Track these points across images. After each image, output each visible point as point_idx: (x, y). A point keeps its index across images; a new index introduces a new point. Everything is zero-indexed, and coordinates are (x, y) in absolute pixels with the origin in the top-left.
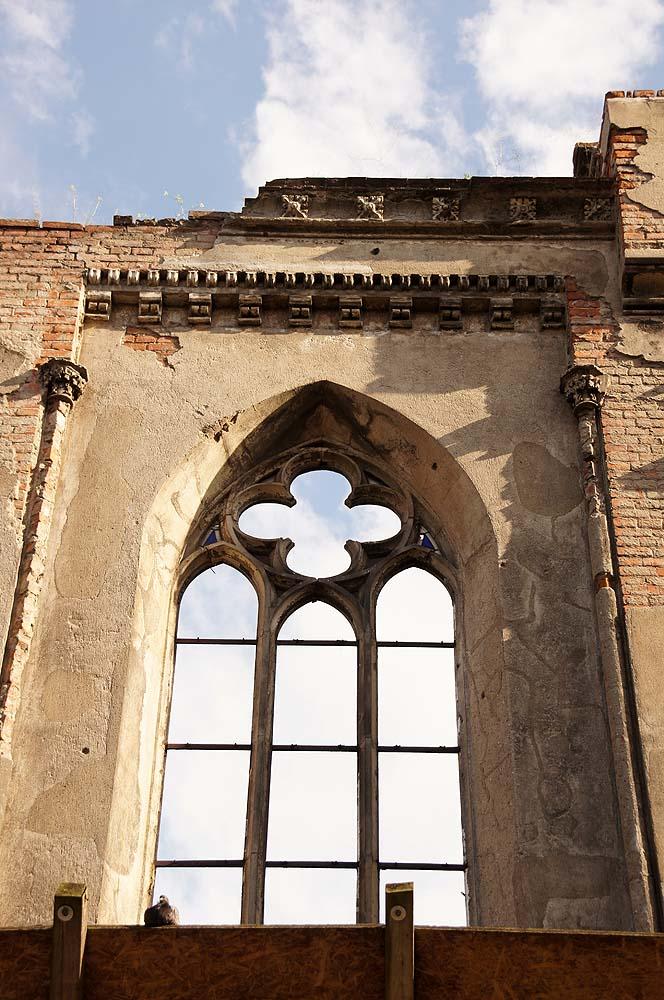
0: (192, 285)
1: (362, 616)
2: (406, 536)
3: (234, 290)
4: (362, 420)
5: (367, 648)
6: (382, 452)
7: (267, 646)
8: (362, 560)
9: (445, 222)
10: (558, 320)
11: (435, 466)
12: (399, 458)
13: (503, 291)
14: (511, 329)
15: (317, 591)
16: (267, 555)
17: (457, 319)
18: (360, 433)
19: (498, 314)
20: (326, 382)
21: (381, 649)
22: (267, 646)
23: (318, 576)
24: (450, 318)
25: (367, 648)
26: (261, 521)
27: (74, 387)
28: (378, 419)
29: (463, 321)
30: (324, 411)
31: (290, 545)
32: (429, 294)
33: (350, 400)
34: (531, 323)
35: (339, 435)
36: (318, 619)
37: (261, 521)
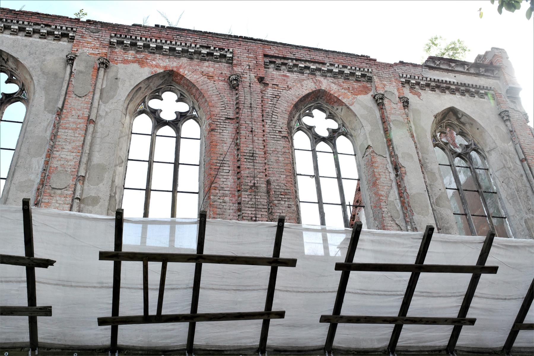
0: (138, 40)
1: (178, 130)
2: (190, 111)
3: (123, 40)
4: (460, 116)
5: (178, 138)
6: (464, 124)
7: (153, 136)
8: (179, 117)
9: (467, 71)
10: (371, 80)
11: (478, 129)
12: (468, 126)
13: (482, 89)
14: (484, 98)
15: (324, 139)
16: (155, 113)
17: (268, 65)
18: (458, 119)
19: (13, 30)
20: (453, 107)
21: (181, 139)
22: (153, 136)
23: (168, 120)
24: (472, 94)
25: (178, 138)
26: (154, 104)
27: (106, 65)
28: (464, 117)
29: (465, 93)
30: (451, 113)
31: (161, 111)
32: (173, 46)
33: (458, 112)
34: (66, 39)
35: (454, 120)
36: (322, 146)
37: (154, 104)
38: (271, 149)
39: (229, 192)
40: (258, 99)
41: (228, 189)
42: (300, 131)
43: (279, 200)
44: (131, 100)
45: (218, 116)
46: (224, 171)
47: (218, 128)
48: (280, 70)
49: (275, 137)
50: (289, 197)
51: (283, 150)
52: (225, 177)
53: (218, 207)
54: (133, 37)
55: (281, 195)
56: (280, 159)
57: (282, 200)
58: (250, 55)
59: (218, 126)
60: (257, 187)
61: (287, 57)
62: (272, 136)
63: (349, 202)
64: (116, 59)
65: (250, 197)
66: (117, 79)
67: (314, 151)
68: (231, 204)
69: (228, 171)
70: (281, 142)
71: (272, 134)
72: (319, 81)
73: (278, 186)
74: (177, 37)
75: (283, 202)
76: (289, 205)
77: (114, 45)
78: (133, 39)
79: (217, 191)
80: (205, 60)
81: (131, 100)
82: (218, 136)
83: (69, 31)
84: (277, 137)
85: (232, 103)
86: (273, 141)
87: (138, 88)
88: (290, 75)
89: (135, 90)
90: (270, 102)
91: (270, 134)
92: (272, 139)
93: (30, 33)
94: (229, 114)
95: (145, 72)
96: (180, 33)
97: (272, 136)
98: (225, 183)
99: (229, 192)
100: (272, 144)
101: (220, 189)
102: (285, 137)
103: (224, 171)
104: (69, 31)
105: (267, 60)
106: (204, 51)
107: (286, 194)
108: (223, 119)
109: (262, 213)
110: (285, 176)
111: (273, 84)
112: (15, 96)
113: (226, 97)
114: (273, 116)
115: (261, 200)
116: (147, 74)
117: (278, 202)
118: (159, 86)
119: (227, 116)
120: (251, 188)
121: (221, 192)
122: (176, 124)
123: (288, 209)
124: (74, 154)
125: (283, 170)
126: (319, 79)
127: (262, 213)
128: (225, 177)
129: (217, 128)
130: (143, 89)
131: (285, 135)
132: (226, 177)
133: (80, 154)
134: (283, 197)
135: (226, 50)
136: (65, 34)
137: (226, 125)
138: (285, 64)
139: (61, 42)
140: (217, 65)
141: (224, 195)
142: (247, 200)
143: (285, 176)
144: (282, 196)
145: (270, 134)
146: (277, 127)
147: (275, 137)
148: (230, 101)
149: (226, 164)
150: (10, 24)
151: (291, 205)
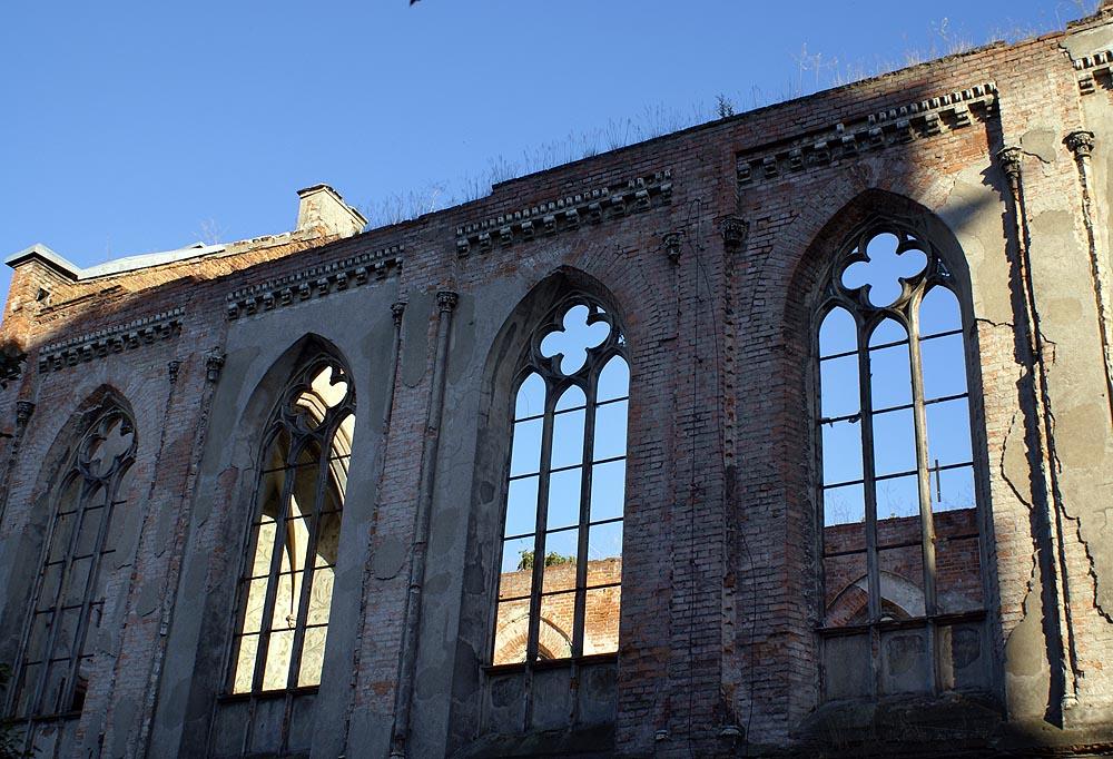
22: (864, 352)
38: (746, 388)
39: (660, 511)
40: (717, 277)
41: (658, 504)
42: (937, 288)
44: (501, 357)
46: (653, 466)
47: (645, 371)
48: (776, 175)
49: (756, 353)
50: (775, 492)
51: (772, 382)
53: (638, 548)
55: (762, 491)
56: (764, 405)
57: (761, 504)
58: (706, 168)
59: (645, 365)
60: (704, 489)
62: (750, 355)
63: (937, 461)
65: (690, 515)
66: (471, 324)
67: (864, 352)
68: (663, 538)
69: (658, 465)
71: (751, 348)
72: (864, 167)
73: (755, 471)
75: (762, 509)
77: (1090, 85)
80: (623, 215)
81: (501, 357)
83: (893, 118)
86: (751, 367)
87: (509, 330)
89: (503, 335)
91: (747, 349)
92: (749, 361)
93: (530, 233)
95: (516, 290)
96: (572, 174)
97: (750, 355)
98: (653, 493)
99: (660, 511)
100: (749, 373)
102: (778, 346)
103: (653, 466)
104: (893, 118)
105: (744, 164)
106: (617, 197)
107: (771, 487)
109: (711, 546)
111: (758, 220)
114: (756, 302)
115: (712, 518)
121: (645, 514)
122: (587, 378)
123: (773, 521)
124: (407, 504)
125: (767, 432)
126: (865, 162)
127: (711, 546)
129: (641, 372)
130: (520, 326)
131: (779, 343)
135: (658, 176)
138: (782, 157)
139: (388, 280)
141: (652, 521)
142: (683, 523)
143: (771, 445)
144: (762, 495)
145: (747, 349)
146: (761, 329)
147: (756, 353)
149: (656, 449)
151: (779, 510)
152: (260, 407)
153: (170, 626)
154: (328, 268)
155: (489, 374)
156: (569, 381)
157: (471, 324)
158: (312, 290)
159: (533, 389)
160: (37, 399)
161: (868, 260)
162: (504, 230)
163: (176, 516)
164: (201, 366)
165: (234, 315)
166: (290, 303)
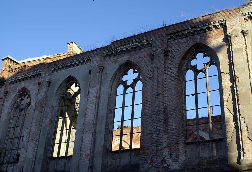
22: (196, 80)
43: (171, 114)
44: (113, 81)
45: (146, 77)
48: (176, 40)
49: (171, 80)
50: (175, 111)
51: (175, 87)
52: (148, 109)
54: (88, 57)
61: (178, 31)
62: (170, 80)
63: (212, 105)
64: (106, 63)
66: (107, 73)
67: (196, 80)
70: (174, 82)
71: (170, 79)
74: (128, 42)
76: (175, 116)
77: (247, 19)
78: (200, 27)
79: (144, 117)
81: (113, 81)
82: (146, 88)
84: (172, 80)
85: (152, 68)
87: (115, 75)
88: (181, 41)
89: (114, 76)
90: (170, 61)
94: (151, 75)
95: (117, 66)
97: (170, 80)
98: (148, 112)
101: (145, 115)
104: (202, 27)
106: (140, 45)
107: (175, 110)
108: (148, 78)
109: (161, 124)
110: (175, 101)
112: (77, 92)
113: (150, 66)
116: (118, 66)
117: (171, 115)
118: (125, 69)
119: (150, 76)
120: (157, 112)
121: (146, 116)
125: (174, 98)
126: (196, 37)
127: (161, 124)
128: (148, 109)
130: (118, 74)
132: (149, 109)
133: (94, 114)
134: (173, 112)
135: (149, 40)
136: (183, 33)
137: (149, 81)
140: (146, 50)
143: (175, 101)
146: (172, 74)
147: (171, 80)
148: (151, 68)
150: (209, 26)
151: (176, 116)
152: (59, 92)
153: (38, 142)
154: (74, 61)
155: (111, 85)
156: (129, 86)
157: (107, 73)
158: (71, 66)
159: (121, 88)
160: (8, 91)
161: (196, 59)
162: (114, 52)
163: (40, 117)
164: (45, 83)
165: (53, 71)
166: (66, 69)
